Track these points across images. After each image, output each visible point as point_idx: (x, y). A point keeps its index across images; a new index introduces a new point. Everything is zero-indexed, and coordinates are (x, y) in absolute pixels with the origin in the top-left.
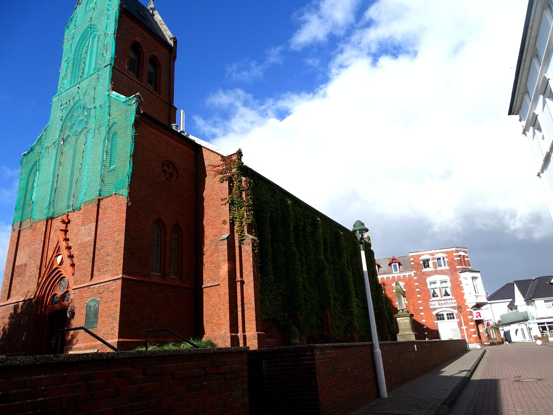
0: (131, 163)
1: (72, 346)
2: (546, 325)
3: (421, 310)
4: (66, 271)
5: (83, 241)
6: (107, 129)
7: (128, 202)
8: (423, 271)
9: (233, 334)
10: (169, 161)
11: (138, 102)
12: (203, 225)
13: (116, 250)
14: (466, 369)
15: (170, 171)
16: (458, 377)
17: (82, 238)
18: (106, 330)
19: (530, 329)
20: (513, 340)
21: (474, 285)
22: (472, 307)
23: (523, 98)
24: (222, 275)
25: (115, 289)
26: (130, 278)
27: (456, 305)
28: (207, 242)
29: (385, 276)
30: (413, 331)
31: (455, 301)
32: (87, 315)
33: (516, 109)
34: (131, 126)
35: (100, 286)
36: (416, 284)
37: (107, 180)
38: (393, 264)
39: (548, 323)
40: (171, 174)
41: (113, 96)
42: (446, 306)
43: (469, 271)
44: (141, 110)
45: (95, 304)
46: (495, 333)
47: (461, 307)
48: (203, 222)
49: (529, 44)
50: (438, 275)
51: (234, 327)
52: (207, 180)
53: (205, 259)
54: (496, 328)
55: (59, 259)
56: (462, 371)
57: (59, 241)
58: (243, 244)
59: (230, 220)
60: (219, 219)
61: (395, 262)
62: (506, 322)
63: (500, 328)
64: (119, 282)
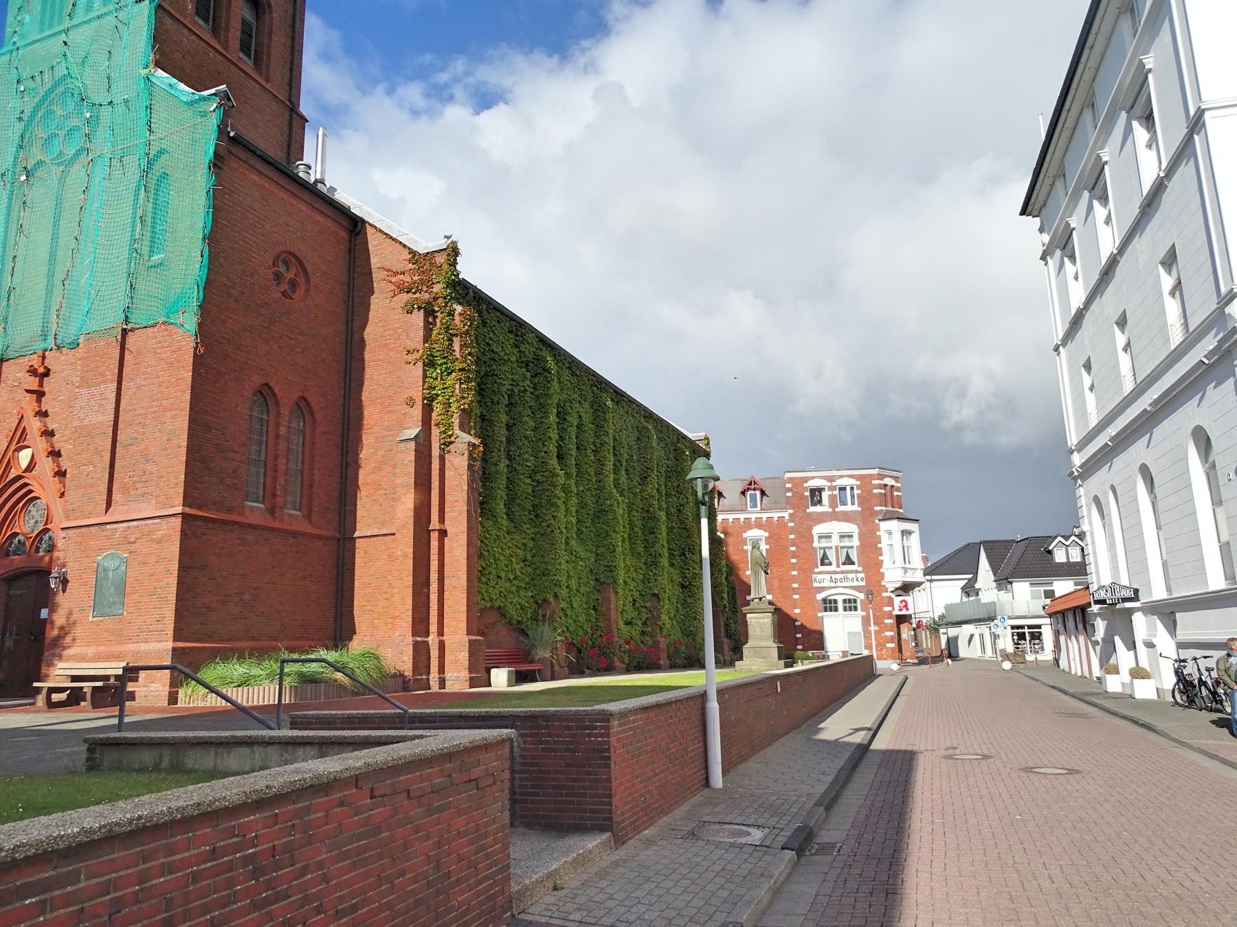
0: (206, 254)
1: (63, 650)
2: (1026, 630)
3: (794, 588)
4: (43, 482)
5: (86, 422)
6: (144, 162)
7: (197, 347)
8: (808, 511)
9: (419, 639)
10: (290, 253)
11: (224, 108)
12: (361, 401)
13: (168, 451)
14: (864, 726)
15: (290, 275)
16: (849, 744)
17: (82, 416)
18: (145, 622)
19: (995, 637)
20: (962, 654)
21: (903, 547)
22: (893, 589)
23: (1052, 185)
24: (400, 514)
25: (164, 536)
26: (201, 513)
27: (863, 583)
28: (368, 440)
29: (731, 517)
30: (776, 640)
31: (863, 575)
32: (98, 586)
33: (1037, 206)
34: (207, 166)
35: (129, 527)
36: (792, 537)
37: (143, 287)
38: (749, 492)
39: (1030, 627)
40: (293, 284)
41: (159, 84)
42: (844, 584)
43: (898, 518)
44: (229, 130)
45: (117, 564)
46: (931, 637)
47: (873, 588)
48: (361, 396)
49: (1082, 80)
50: (836, 522)
51: (420, 624)
52: (374, 300)
53: (363, 477)
54: (935, 627)
55: (24, 457)
56: (857, 730)
57: (22, 417)
58: (449, 452)
59: (424, 399)
60: (398, 392)
61: (755, 489)
62: (954, 620)
63: (942, 631)
64: (177, 523)
